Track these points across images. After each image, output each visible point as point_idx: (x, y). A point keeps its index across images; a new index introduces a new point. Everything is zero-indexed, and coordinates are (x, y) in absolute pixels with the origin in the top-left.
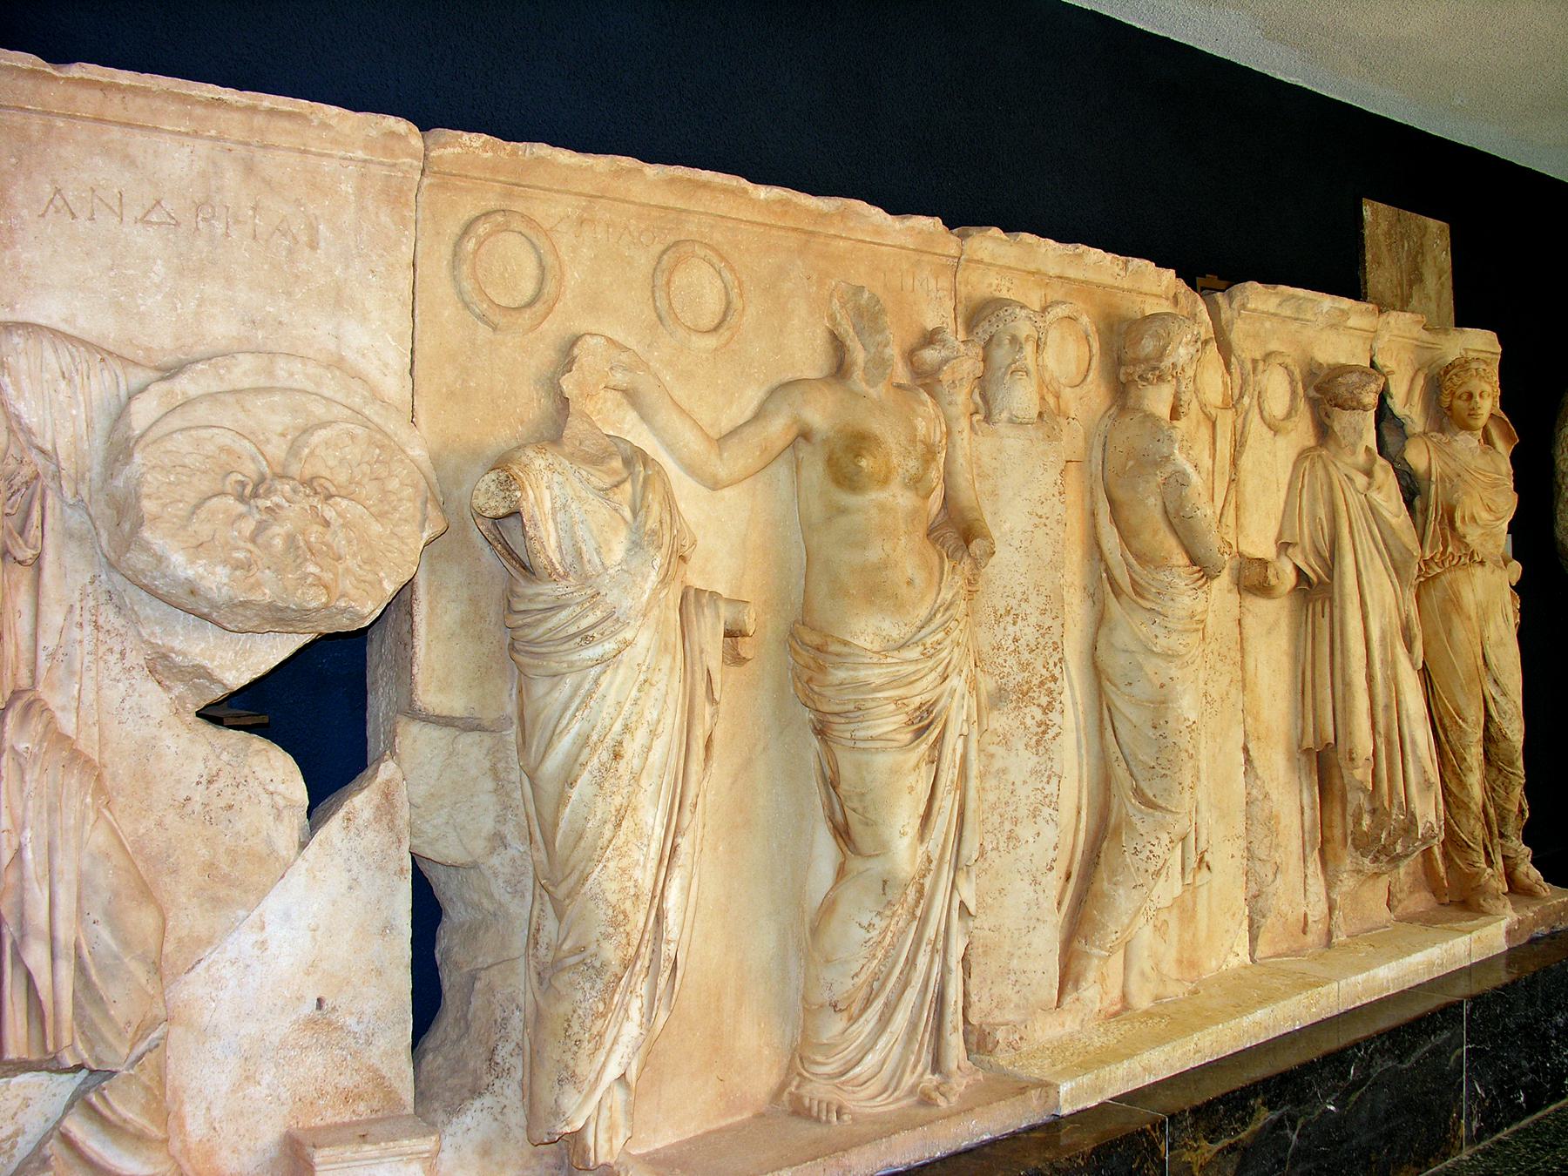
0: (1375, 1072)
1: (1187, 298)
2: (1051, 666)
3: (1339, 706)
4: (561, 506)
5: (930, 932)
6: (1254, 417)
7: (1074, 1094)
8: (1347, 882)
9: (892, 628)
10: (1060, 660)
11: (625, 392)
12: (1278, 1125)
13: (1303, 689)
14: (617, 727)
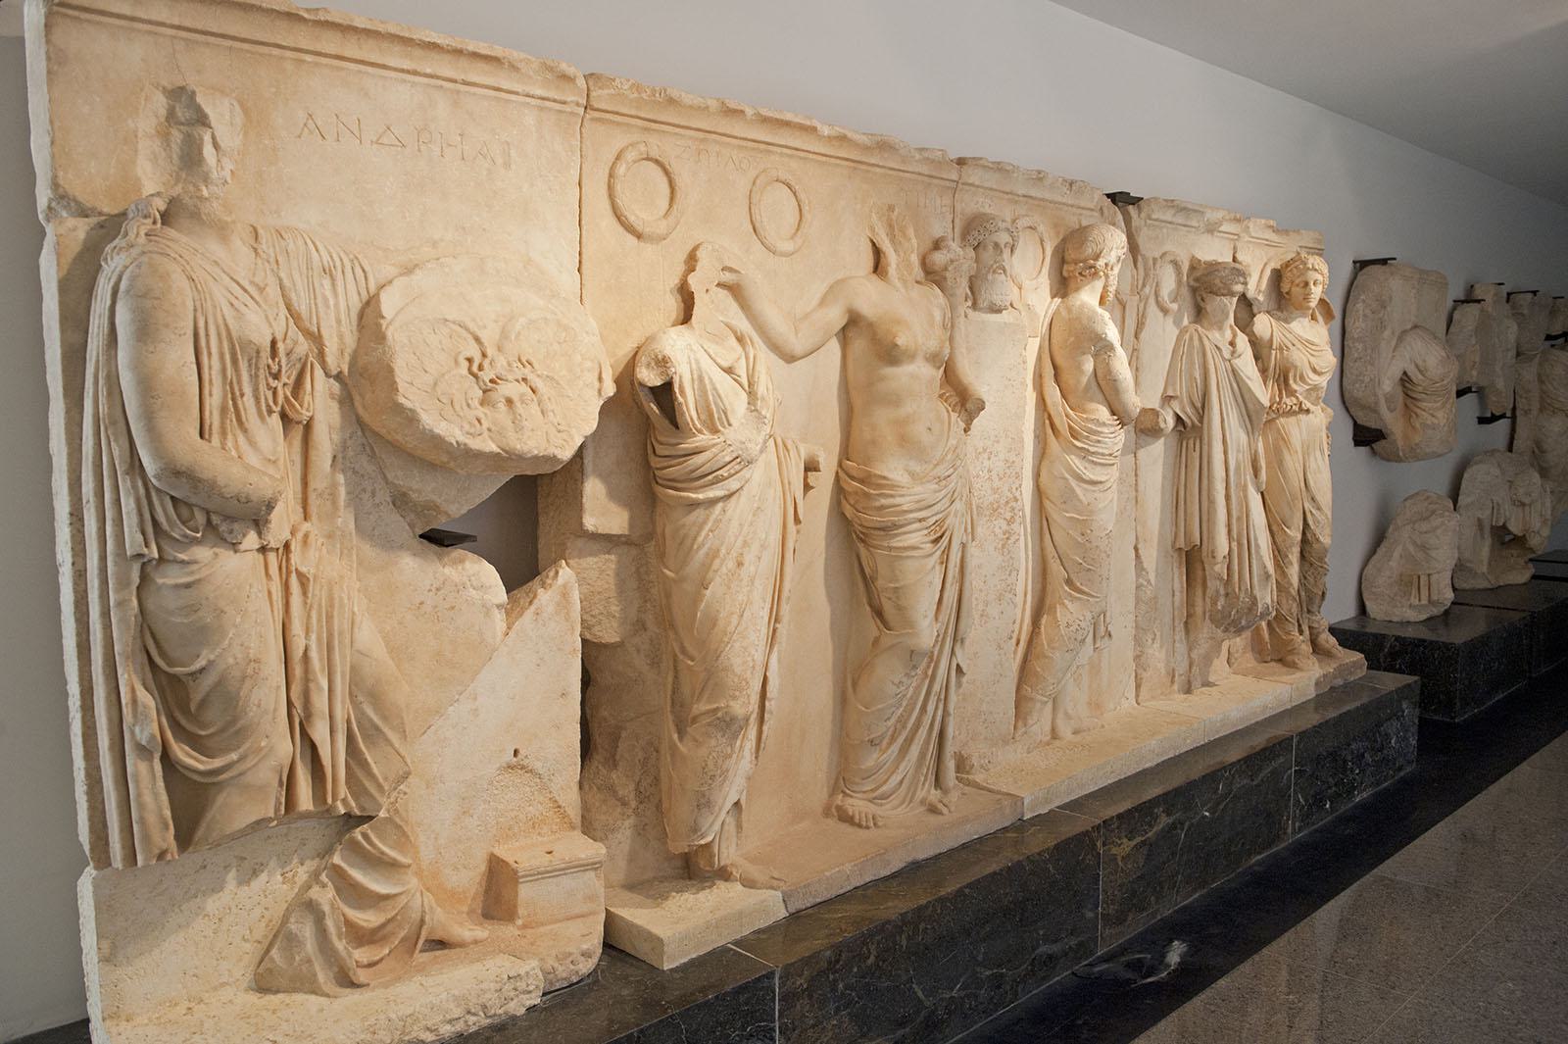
0: (1235, 787)
1: (1108, 208)
2: (1014, 490)
3: (1205, 518)
5: (936, 687)
6: (1152, 301)
7: (1035, 800)
12: (1173, 827)
13: (1177, 503)
14: (739, 542)
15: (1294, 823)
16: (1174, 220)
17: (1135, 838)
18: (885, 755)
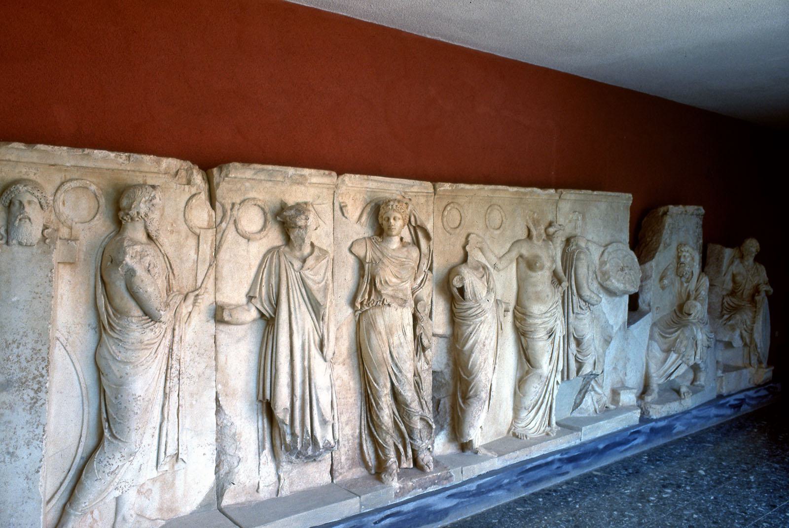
2: (40, 369)
4: (471, 280)
5: (549, 389)
8: (286, 467)
9: (543, 308)
10: (46, 366)
11: (480, 248)
16: (255, 177)
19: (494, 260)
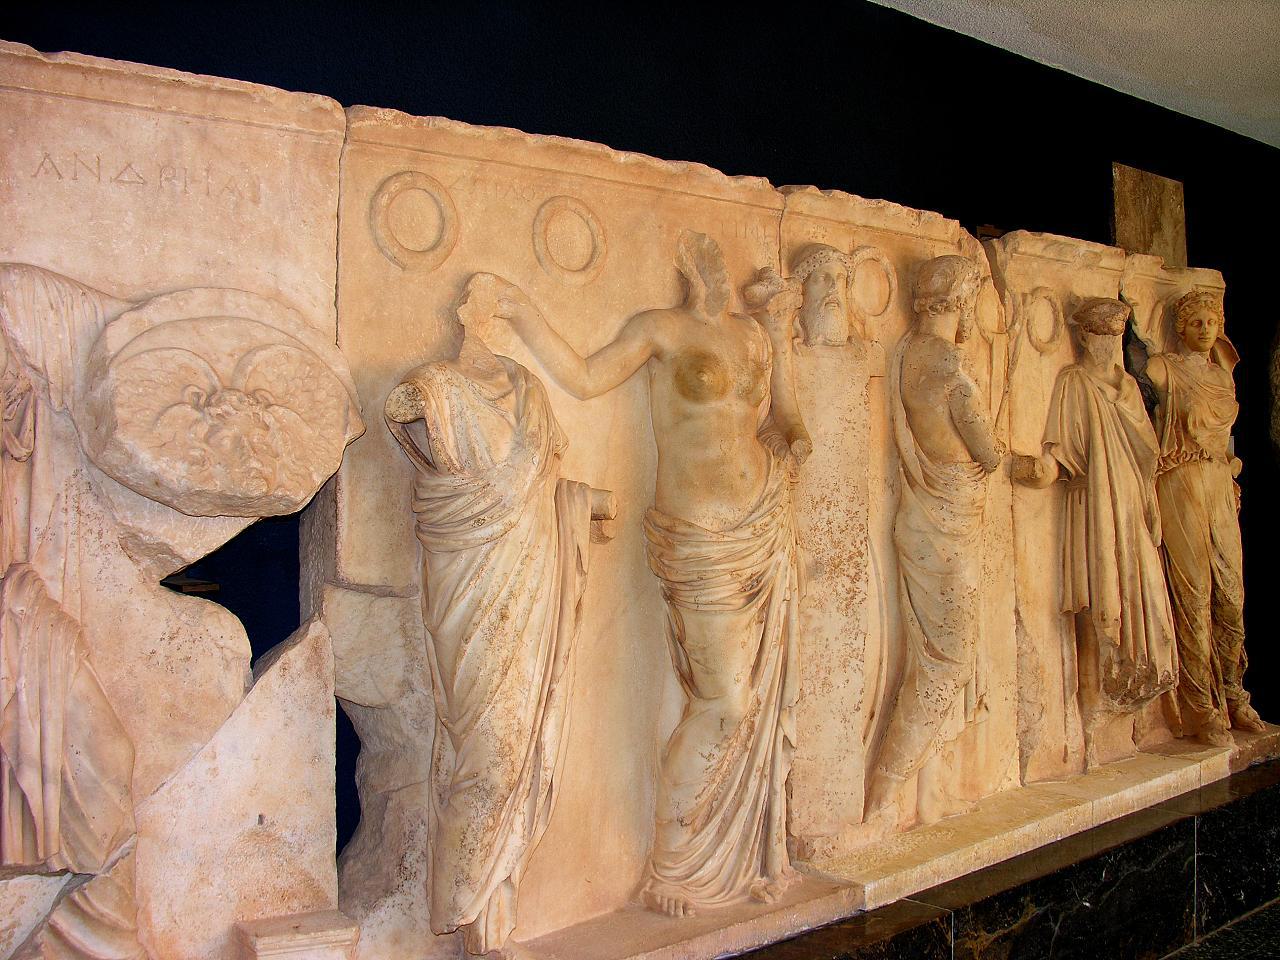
3: (1093, 576)
4: (457, 413)
5: (759, 761)
7: (877, 893)
8: (1100, 720)
9: (728, 513)
13: (1064, 562)
14: (504, 594)
15: (1199, 919)
16: (1044, 254)
17: (996, 930)
18: (698, 838)
19: (566, 361)
